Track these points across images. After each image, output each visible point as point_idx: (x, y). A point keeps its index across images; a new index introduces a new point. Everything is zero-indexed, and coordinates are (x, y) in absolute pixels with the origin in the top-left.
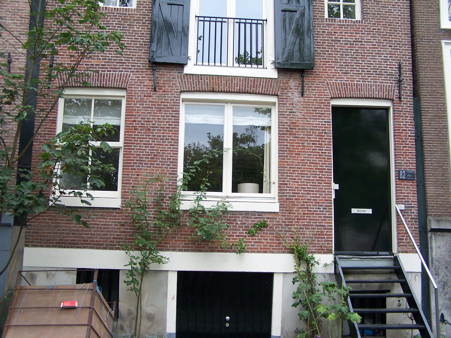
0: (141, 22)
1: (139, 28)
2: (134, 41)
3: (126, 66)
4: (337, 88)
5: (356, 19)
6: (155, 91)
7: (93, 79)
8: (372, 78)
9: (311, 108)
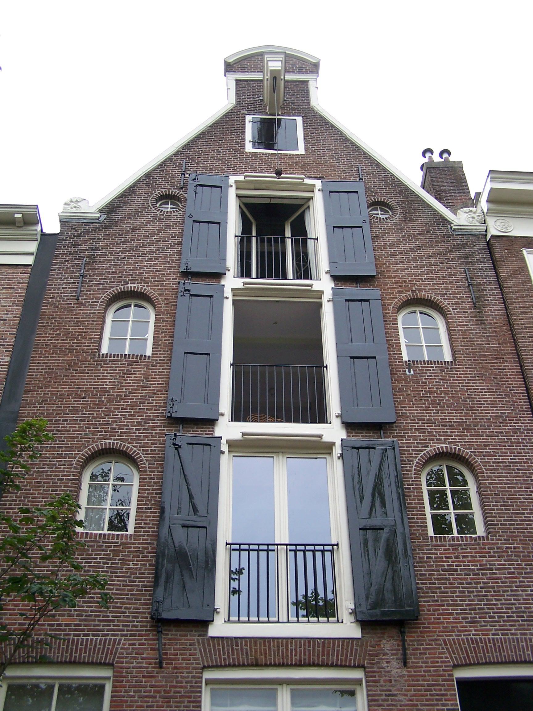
0: (141, 555)
1: (137, 565)
2: (128, 585)
3: (114, 625)
4: (461, 649)
5: (478, 535)
6: (161, 667)
7: (59, 649)
8: (517, 627)
9: (422, 685)
